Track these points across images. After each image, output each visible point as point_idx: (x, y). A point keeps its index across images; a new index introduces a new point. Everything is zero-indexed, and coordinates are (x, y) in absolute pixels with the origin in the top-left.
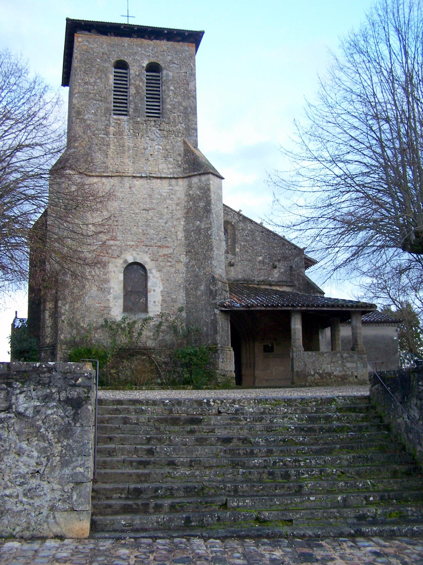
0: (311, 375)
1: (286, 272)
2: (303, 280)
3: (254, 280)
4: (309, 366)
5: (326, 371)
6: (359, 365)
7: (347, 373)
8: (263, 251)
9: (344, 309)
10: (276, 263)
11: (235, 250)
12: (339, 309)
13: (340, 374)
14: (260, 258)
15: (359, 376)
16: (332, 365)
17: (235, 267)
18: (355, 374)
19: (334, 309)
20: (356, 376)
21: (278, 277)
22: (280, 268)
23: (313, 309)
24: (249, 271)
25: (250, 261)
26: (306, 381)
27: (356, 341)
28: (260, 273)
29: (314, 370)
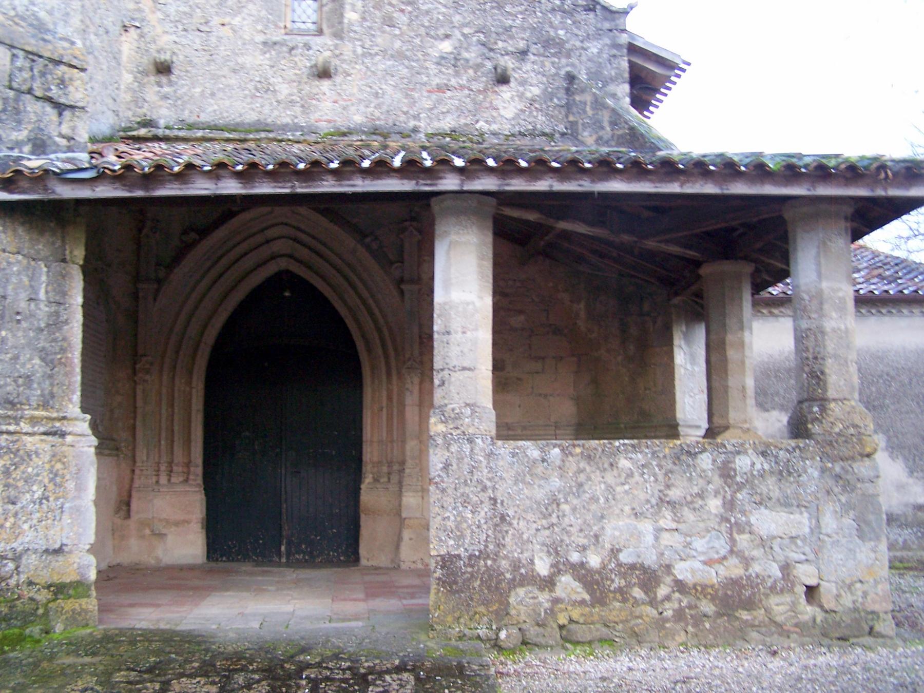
0: (531, 579)
1: (548, 96)
2: (613, 124)
3: (415, 130)
4: (525, 526)
5: (624, 557)
6: (829, 522)
7: (756, 568)
8: (457, 19)
9: (739, 188)
10: (508, 63)
11: (342, 15)
12: (710, 189)
13: (713, 576)
14: (446, 46)
15: (828, 590)
16: (666, 521)
17: (338, 79)
18: (807, 574)
19: (674, 188)
20: (811, 591)
21: (517, 116)
22: (523, 83)
23: (542, 185)
24: (392, 95)
25: (399, 56)
26: (502, 614)
27: (818, 377)
28: (439, 101)
29: (554, 549)
